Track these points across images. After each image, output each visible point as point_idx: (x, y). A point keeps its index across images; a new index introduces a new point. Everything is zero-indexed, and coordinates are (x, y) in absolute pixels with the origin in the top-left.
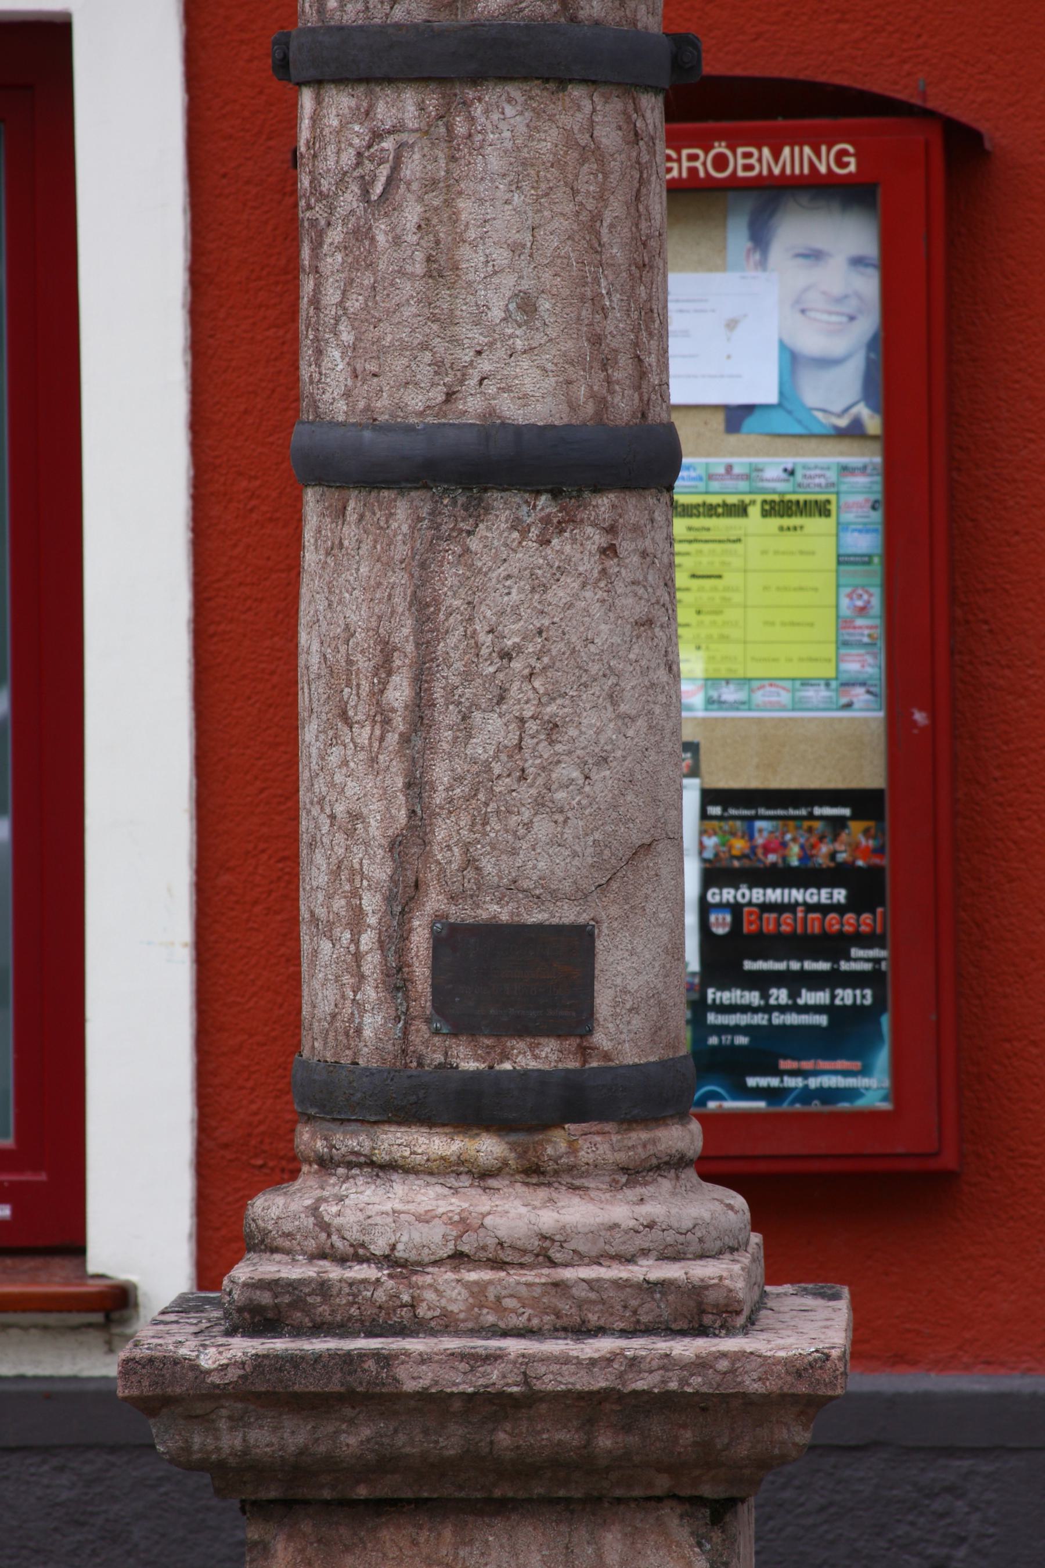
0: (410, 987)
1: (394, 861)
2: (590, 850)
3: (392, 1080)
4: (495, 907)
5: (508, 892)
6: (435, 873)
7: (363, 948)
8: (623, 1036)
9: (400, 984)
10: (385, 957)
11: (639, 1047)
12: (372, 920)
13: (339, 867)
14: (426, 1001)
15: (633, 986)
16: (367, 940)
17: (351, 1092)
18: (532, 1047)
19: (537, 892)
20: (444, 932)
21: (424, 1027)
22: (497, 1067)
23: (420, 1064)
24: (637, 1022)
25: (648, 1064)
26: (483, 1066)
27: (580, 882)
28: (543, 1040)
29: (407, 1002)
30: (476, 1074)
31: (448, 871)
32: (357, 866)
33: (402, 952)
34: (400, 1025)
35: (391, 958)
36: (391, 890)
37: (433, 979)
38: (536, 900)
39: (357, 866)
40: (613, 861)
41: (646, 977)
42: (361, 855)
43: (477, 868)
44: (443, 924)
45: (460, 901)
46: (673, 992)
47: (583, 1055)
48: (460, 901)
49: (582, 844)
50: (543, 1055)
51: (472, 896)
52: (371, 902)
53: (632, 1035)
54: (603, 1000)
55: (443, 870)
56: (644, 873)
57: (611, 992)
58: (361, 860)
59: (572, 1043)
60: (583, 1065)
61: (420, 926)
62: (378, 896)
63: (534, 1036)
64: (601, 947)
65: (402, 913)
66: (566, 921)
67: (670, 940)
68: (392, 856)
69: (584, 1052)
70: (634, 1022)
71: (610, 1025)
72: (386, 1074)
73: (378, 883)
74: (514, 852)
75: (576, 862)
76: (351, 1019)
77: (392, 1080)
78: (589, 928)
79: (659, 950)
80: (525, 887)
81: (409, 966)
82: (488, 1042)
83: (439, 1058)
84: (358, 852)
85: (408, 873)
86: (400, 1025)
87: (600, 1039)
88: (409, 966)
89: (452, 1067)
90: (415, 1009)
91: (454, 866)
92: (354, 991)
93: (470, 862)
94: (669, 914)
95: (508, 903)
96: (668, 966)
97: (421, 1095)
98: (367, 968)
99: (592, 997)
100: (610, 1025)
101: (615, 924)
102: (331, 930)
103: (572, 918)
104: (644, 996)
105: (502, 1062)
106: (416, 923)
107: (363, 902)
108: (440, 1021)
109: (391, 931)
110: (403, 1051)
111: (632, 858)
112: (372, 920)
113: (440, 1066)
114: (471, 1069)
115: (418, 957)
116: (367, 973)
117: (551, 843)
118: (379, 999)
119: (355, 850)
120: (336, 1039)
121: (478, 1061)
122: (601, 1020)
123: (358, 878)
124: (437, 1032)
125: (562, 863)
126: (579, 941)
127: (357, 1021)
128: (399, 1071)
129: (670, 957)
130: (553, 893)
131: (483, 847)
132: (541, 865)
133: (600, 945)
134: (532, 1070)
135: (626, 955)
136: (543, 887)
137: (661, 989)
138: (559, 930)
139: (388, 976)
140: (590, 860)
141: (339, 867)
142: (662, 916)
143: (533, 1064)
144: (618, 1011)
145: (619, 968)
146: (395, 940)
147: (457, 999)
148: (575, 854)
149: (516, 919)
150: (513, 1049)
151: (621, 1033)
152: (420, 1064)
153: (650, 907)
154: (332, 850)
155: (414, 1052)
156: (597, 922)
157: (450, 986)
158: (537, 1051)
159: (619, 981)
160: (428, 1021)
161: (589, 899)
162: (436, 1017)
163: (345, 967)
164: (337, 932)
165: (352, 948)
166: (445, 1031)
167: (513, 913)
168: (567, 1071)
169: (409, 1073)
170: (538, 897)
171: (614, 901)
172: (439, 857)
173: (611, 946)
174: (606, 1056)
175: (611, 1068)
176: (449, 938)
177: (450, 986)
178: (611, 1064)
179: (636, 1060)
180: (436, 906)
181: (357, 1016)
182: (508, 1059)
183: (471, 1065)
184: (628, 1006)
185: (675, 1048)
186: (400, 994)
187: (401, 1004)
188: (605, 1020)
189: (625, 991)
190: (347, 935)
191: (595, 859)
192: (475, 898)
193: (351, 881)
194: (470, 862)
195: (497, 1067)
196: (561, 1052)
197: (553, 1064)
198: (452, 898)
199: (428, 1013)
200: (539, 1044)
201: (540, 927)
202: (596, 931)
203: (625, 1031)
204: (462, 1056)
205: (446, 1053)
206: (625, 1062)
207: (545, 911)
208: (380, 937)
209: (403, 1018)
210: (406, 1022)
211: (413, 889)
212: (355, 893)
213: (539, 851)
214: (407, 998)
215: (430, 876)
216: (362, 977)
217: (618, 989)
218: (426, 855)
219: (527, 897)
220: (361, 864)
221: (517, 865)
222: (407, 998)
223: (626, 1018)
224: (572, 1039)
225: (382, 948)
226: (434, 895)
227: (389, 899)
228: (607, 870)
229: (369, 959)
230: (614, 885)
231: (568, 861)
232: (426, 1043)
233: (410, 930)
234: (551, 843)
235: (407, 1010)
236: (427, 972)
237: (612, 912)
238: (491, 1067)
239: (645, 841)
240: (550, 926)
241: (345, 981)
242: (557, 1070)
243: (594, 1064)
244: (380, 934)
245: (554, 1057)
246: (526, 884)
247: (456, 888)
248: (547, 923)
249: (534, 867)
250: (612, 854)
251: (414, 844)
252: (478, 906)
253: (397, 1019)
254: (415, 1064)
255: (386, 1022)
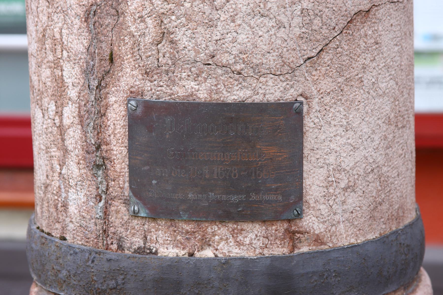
0: (109, 166)
1: (90, 32)
2: (297, 20)
3: (93, 261)
4: (193, 84)
5: (206, 67)
6: (129, 46)
7: (66, 122)
8: (337, 217)
9: (99, 161)
10: (85, 133)
11: (356, 227)
12: (73, 93)
13: (44, 36)
14: (124, 182)
15: (348, 163)
16: (70, 113)
17: (58, 268)
18: (234, 234)
19: (238, 67)
20: (139, 111)
21: (123, 209)
22: (198, 255)
23: (120, 247)
24: (353, 200)
25: (365, 244)
26: (183, 252)
27: (286, 55)
28: (247, 226)
29: (107, 181)
30: (175, 263)
31: (142, 44)
32: (58, 36)
33: (99, 129)
34: (101, 204)
35: (90, 135)
36: (87, 63)
37: (129, 158)
38: (237, 76)
39: (58, 36)
40: (325, 31)
41: (364, 152)
42: (60, 25)
43: (172, 42)
44: (138, 102)
45: (155, 77)
46: (398, 162)
47: (292, 239)
48: (155, 77)
49: (288, 13)
50: (247, 241)
51: (167, 72)
52: (72, 74)
53: (347, 215)
54: (313, 181)
55: (136, 44)
56: (361, 42)
57: (323, 172)
58: (61, 29)
59: (280, 228)
60: (292, 251)
61: (116, 102)
62: (77, 68)
63: (236, 221)
64: (312, 125)
65: (99, 87)
66: (271, 98)
67: (392, 110)
68: (88, 27)
69: (292, 236)
70: (350, 201)
71: (322, 207)
72: (87, 255)
73: (76, 55)
74: (211, 24)
75: (282, 33)
76: (58, 194)
77: (93, 261)
78: (297, 105)
79: (380, 122)
80: (224, 61)
81: (107, 144)
82: (188, 227)
83: (138, 242)
84: (58, 18)
85: (104, 45)
86: (101, 204)
87: (311, 222)
88: (107, 144)
89: (151, 253)
90: (114, 192)
91: (148, 39)
92: (60, 165)
93: (164, 35)
94: (392, 83)
95: (206, 79)
96: (390, 137)
97: (120, 282)
98: (70, 143)
99: (301, 178)
100: (322, 207)
101: (327, 99)
102: (41, 99)
103: (278, 95)
104: (362, 172)
105: (202, 249)
106: (112, 99)
107: (64, 73)
108: (137, 204)
109: (89, 106)
110: (105, 231)
111: (347, 27)
112: (73, 93)
113: (140, 251)
114: (171, 255)
115: (115, 135)
116: (70, 148)
117: (253, 14)
118: (81, 175)
119: (55, 18)
120: (49, 211)
121: (177, 247)
122: (311, 202)
123: (59, 48)
124: (135, 215)
125: (266, 36)
126: (287, 120)
127: (64, 195)
128: (99, 253)
129: (393, 127)
130: (256, 68)
131: (178, 19)
132: (242, 38)
133: (309, 123)
134: (235, 259)
135: (340, 131)
136: (244, 62)
137: (382, 162)
138: (262, 108)
139: (88, 152)
140: (297, 31)
141: (44, 36)
142: (383, 85)
143: (236, 252)
144: (331, 191)
145: (332, 146)
146: (94, 116)
147: (154, 182)
148: (280, 25)
149: (215, 97)
150: (214, 235)
151: (335, 214)
152: (120, 247)
153: (368, 78)
154: (38, 17)
155: (114, 233)
156: (306, 98)
157: (147, 168)
158: (240, 238)
159: (331, 159)
160: (127, 202)
161: (297, 73)
162: (134, 199)
163: (52, 139)
164: (46, 100)
165: (57, 121)
166: (142, 215)
167: (212, 91)
168: (274, 258)
169: (108, 257)
170: (239, 73)
171: (326, 75)
172: (133, 29)
173: (322, 123)
174: (318, 240)
175: (323, 252)
176: (146, 118)
177: (147, 168)
178: (324, 247)
179: (353, 241)
180: (131, 81)
181: (63, 190)
182: (210, 245)
183: (169, 251)
184: (343, 185)
185: (398, 218)
186: (100, 173)
187: (101, 183)
188: (316, 201)
189: (339, 169)
190: (52, 107)
191: (304, 30)
192: (170, 74)
193: (54, 51)
194: (164, 35)
195: (198, 255)
196: (267, 238)
197: (258, 251)
198: (146, 73)
199: (126, 194)
200: (242, 230)
201: (241, 107)
202: (305, 108)
203: (340, 211)
204: (161, 241)
205: (145, 237)
206: (340, 244)
207: (247, 88)
208: (79, 112)
209: (104, 197)
210: (106, 202)
211: (108, 62)
212: (57, 65)
213: (239, 22)
214: (106, 177)
215: (124, 50)
216: (66, 151)
217: (331, 168)
218: (119, 26)
219: (227, 72)
220: (61, 33)
221: (215, 38)
222: (106, 177)
223: (340, 198)
224: (279, 224)
225: (81, 122)
226: (128, 70)
227: (87, 72)
228: (318, 41)
229: (71, 133)
230: (326, 57)
231: (272, 32)
232: (125, 225)
233: (107, 107)
234: (253, 14)
235: (107, 189)
236: (125, 151)
237: (324, 87)
238: (191, 255)
239: (362, 8)
240: (253, 105)
241: (53, 154)
242: (262, 258)
243: (305, 249)
244: (79, 108)
245: (258, 244)
246: (225, 59)
247: (151, 62)
248: (250, 101)
249: (234, 41)
250: (324, 24)
251: (107, 14)
252: (174, 83)
253: (99, 198)
254: (115, 247)
255: (88, 200)
